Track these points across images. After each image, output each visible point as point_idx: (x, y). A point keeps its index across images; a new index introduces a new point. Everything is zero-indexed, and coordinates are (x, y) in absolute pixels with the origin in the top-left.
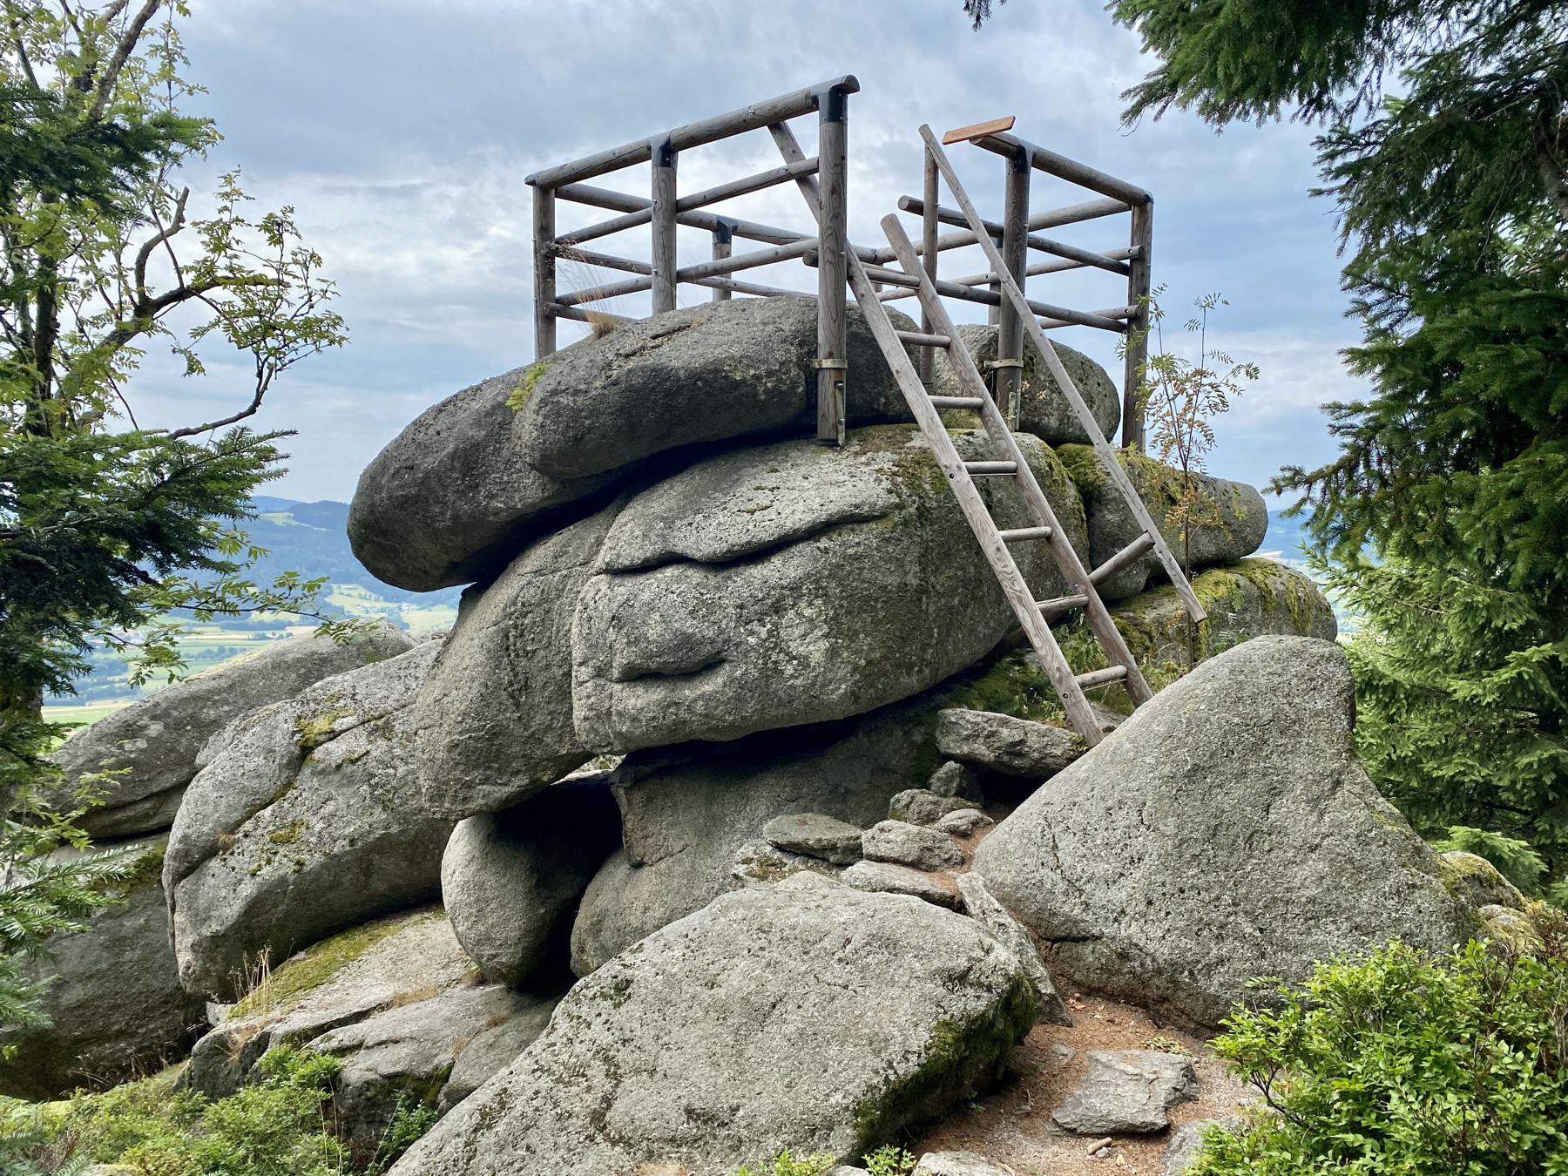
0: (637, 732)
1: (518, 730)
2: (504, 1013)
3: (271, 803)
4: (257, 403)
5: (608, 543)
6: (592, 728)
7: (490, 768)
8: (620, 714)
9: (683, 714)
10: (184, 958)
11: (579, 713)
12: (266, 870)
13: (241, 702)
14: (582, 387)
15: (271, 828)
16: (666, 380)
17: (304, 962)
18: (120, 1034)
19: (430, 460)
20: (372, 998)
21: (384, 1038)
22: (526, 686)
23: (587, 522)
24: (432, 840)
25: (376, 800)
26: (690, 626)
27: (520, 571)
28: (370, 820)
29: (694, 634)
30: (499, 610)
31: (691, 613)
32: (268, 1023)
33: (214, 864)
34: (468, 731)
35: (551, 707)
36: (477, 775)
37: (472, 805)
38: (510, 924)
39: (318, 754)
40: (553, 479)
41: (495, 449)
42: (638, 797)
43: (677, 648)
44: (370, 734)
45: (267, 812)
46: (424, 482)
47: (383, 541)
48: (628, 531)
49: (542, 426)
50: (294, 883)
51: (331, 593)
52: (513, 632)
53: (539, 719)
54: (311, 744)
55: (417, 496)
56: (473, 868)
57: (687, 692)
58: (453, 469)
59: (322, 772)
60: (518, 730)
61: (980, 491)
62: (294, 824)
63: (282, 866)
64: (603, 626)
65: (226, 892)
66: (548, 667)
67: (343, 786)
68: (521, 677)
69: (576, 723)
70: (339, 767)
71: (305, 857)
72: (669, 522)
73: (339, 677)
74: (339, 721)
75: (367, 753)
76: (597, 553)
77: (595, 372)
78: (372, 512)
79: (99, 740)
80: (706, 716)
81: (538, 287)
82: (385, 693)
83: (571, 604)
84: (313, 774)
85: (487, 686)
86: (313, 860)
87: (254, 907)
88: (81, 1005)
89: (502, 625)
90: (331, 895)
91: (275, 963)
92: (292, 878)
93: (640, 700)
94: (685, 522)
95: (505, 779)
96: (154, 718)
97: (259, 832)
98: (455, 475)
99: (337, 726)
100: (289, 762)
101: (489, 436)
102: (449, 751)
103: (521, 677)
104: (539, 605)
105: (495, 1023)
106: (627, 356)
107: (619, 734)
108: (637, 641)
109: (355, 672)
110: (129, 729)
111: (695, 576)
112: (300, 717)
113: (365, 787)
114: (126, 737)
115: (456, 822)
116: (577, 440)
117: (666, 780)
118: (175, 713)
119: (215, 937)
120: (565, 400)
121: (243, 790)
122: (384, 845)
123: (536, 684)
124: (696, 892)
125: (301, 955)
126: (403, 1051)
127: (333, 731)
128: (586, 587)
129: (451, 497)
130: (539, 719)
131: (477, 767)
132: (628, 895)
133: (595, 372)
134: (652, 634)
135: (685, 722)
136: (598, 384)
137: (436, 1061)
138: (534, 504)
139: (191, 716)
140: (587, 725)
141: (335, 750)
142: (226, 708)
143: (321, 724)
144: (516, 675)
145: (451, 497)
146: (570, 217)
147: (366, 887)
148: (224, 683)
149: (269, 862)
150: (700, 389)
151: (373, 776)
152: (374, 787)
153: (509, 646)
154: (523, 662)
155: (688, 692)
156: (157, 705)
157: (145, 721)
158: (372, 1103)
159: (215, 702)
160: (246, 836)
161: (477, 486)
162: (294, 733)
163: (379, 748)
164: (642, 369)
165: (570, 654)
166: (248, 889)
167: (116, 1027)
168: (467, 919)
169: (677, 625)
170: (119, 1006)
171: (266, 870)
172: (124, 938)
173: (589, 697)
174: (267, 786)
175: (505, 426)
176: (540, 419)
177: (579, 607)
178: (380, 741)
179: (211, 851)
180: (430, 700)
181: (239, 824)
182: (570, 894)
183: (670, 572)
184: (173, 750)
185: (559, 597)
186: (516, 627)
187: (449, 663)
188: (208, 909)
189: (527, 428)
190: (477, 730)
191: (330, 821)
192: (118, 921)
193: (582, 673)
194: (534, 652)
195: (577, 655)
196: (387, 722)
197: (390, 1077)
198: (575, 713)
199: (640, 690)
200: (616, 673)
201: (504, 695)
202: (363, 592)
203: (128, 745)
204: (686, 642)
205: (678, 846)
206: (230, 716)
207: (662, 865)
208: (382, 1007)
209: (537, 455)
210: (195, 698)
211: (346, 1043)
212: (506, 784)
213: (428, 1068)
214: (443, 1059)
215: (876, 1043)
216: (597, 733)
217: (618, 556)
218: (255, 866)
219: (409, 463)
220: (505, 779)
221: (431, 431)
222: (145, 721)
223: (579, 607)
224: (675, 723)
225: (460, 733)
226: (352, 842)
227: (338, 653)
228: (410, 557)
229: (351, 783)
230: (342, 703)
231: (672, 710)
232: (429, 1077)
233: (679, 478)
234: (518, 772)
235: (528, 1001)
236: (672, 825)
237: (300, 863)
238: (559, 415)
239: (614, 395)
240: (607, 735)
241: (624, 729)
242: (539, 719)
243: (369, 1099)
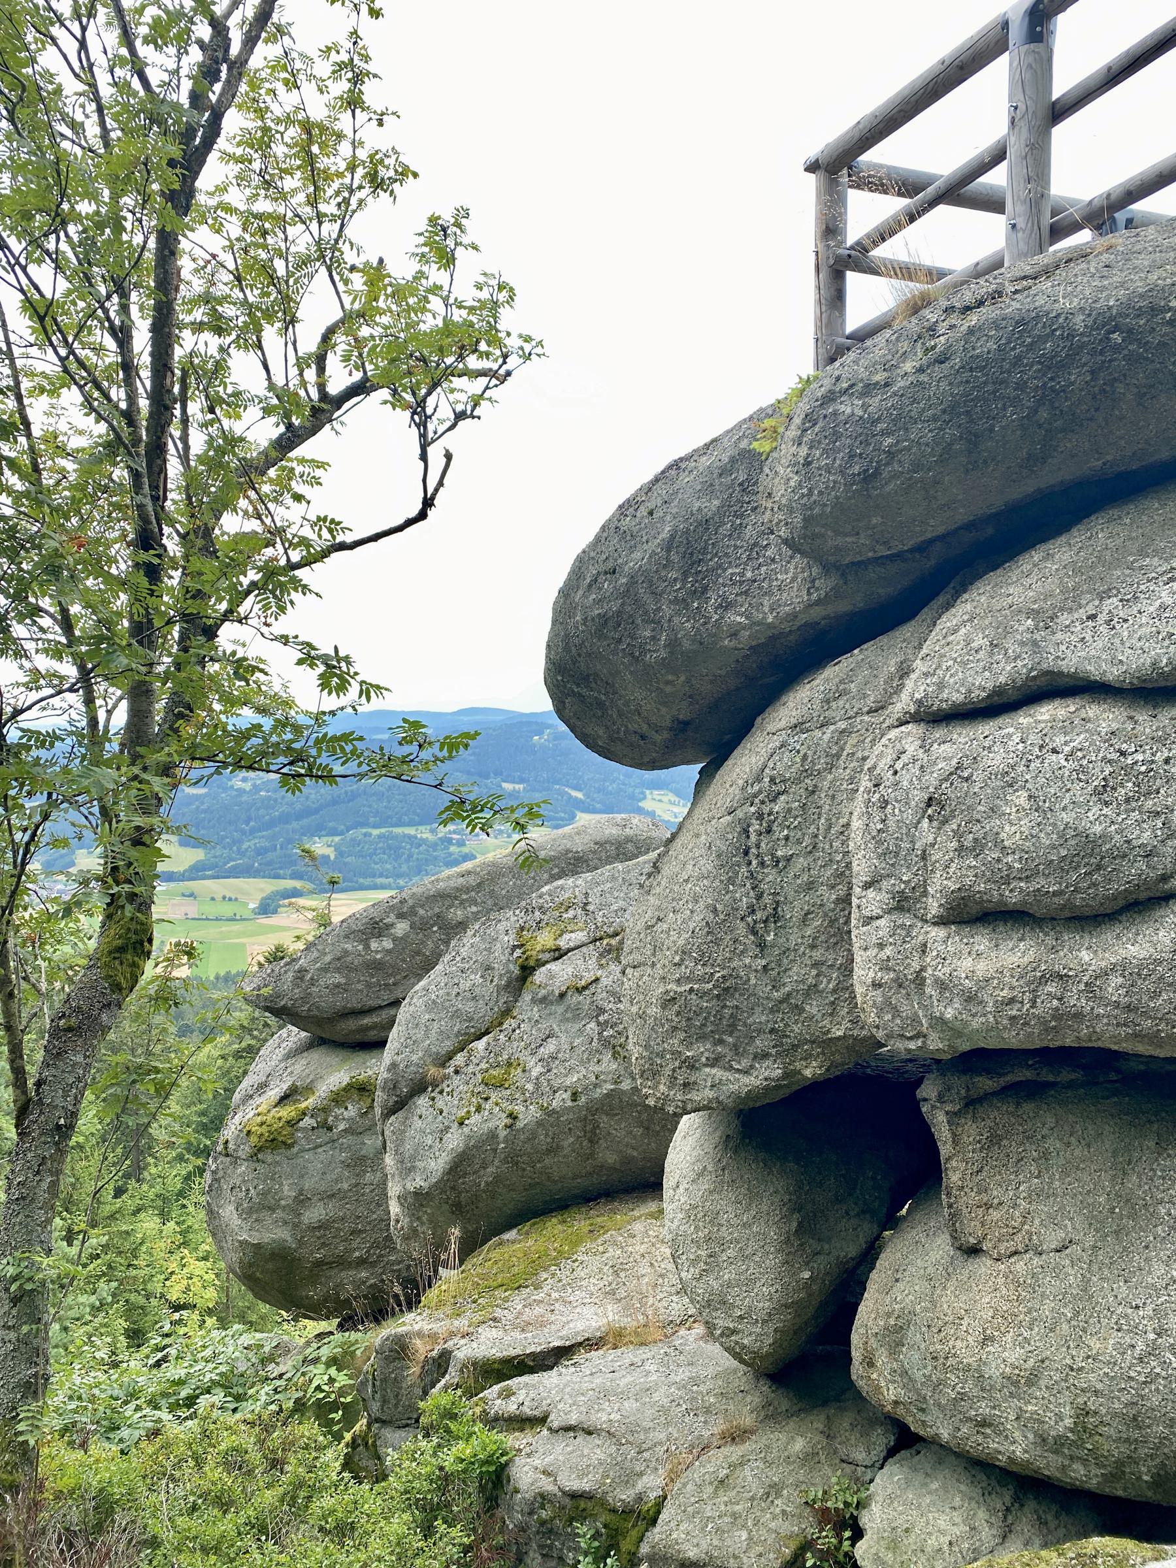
0: (976, 1023)
1: (763, 988)
2: (748, 1421)
3: (487, 1032)
4: (428, 503)
5: (919, 666)
6: (887, 1002)
7: (721, 1042)
8: (942, 986)
9: (1075, 999)
10: (394, 1208)
11: (863, 973)
12: (475, 1119)
13: (490, 902)
14: (879, 377)
15: (484, 1066)
16: (1043, 339)
17: (515, 1245)
18: (362, 1262)
19: (637, 555)
20: (580, 1326)
21: (573, 1420)
22: (776, 916)
23: (883, 640)
24: (662, 1125)
25: (606, 1043)
26: (1095, 820)
27: (771, 728)
28: (597, 1069)
29: (1105, 837)
30: (735, 791)
31: (1096, 792)
32: (452, 1334)
33: (422, 1101)
34: (688, 979)
35: (817, 954)
36: (702, 1050)
37: (695, 1096)
38: (762, 1284)
39: (539, 976)
40: (827, 568)
41: (734, 528)
42: (971, 1131)
43: (1068, 864)
44: (601, 955)
45: (481, 1045)
46: (627, 592)
47: (584, 691)
48: (961, 645)
49: (807, 463)
50: (506, 1140)
51: (645, 798)
52: (755, 826)
53: (797, 974)
54: (532, 963)
55: (619, 613)
56: (705, 1185)
57: (1085, 956)
58: (668, 564)
59: (544, 1000)
60: (763, 988)
61: (290, 1088)
62: (509, 1064)
63: (491, 1119)
64: (909, 816)
65: (427, 1145)
66: (810, 886)
67: (568, 1020)
68: (767, 899)
69: (859, 990)
70: (562, 995)
71: (519, 1108)
72: (1045, 619)
73: (570, 881)
74: (566, 936)
75: (597, 980)
76: (898, 690)
77: (905, 346)
78: (567, 649)
79: (347, 937)
80: (1129, 1008)
81: (819, 319)
82: (621, 903)
83: (851, 780)
84: (534, 1001)
85: (715, 911)
86: (529, 1115)
87: (460, 1165)
88: (323, 1226)
89: (740, 814)
90: (547, 1161)
91: (469, 1247)
92: (503, 1134)
93: (990, 964)
94: (1082, 614)
95: (745, 1063)
96: (401, 916)
97: (471, 1069)
98: (673, 575)
99: (563, 943)
100: (508, 985)
101: (726, 505)
102: (664, 1007)
103: (767, 899)
104: (797, 781)
105: (734, 1436)
106: (967, 309)
107: (939, 1022)
108: (978, 848)
109: (588, 876)
110: (374, 927)
111: (1106, 717)
112: (522, 929)
113: (593, 1025)
114: (373, 935)
115: (677, 1117)
116: (868, 478)
117: (1028, 1107)
118: (421, 912)
119: (417, 1194)
120: (847, 407)
121: (457, 1014)
122: (614, 1104)
123: (792, 912)
124: (1095, 1345)
125: (511, 1235)
126: (595, 1451)
127: (558, 949)
128: (878, 749)
129: (667, 610)
130: (797, 974)
131: (702, 1038)
132: (950, 1301)
133: (905, 346)
134: (1010, 834)
135: (1078, 1016)
136: (908, 366)
137: (640, 1486)
138: (794, 616)
140: (878, 996)
141: (557, 974)
142: (474, 909)
143: (545, 939)
144: (759, 897)
145: (667, 610)
146: (865, 212)
147: (591, 1155)
148: (472, 881)
149: (479, 1109)
150: (1117, 348)
151: (602, 1011)
152: (603, 1026)
153: (745, 852)
154: (771, 875)
155: (1087, 954)
156: (403, 901)
157: (391, 919)
158: (547, 1529)
160: (457, 1072)
161: (705, 589)
162: (515, 947)
163: (610, 975)
164: (996, 324)
165: (849, 865)
166: (455, 1140)
167: (357, 1254)
168: (694, 1262)
169: (1067, 817)
170: (360, 1231)
171: (475, 1119)
172: (364, 1158)
173: (881, 946)
174: (483, 1012)
175: (748, 487)
176: (804, 451)
177: (865, 783)
178: (612, 967)
179: (420, 1087)
180: (640, 926)
181: (450, 1056)
182: (852, 1250)
183: (1046, 712)
184: (418, 953)
185: (830, 767)
186: (760, 816)
187: (667, 870)
188: (413, 1158)
189: (781, 482)
190: (701, 980)
191: (551, 1068)
192: (359, 1139)
193: (870, 901)
194: (789, 859)
195: (861, 869)
197: (574, 1496)
198: (858, 972)
199: (982, 941)
200: (933, 907)
201: (741, 929)
202: (673, 798)
203: (374, 945)
204: (1088, 850)
205: (1053, 1238)
206: (476, 917)
207: (1020, 1266)
208: (592, 1344)
209: (798, 520)
210: (441, 896)
211: (527, 1411)
212: (746, 1072)
213: (625, 1495)
214: (651, 1484)
216: (896, 1012)
217: (941, 686)
218: (462, 1113)
219: (610, 564)
220: (745, 1063)
221: (643, 511)
222: (391, 919)
223: (865, 783)
224: (1057, 1015)
225: (678, 982)
226: (575, 1096)
227: (595, 852)
228: (620, 714)
229: (577, 1018)
230: (571, 913)
231: (1051, 988)
232: (627, 1512)
233: (1063, 539)
234: (765, 1056)
235: (785, 1405)
236: (1035, 1195)
237: (513, 1116)
238: (837, 436)
239: (940, 384)
240: (915, 1019)
241: (949, 1014)
242: (796, 972)
243: (543, 1523)
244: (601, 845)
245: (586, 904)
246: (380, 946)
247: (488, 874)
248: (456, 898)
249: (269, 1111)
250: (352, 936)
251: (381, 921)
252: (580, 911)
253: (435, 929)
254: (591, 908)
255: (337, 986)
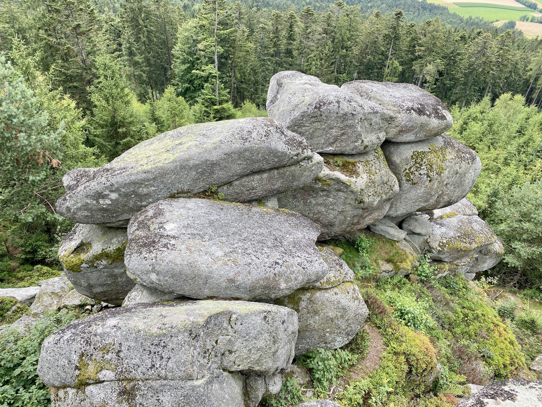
79: (87, 197)
96: (112, 191)
99: (101, 376)
118: (123, 190)
139: (133, 191)
142: (153, 188)
148: (150, 176)
159: (146, 185)
196: (133, 388)
203: (101, 202)
210: (134, 183)
215: (348, 88)
244: (229, 155)
245: (119, 351)
246: (105, 203)
247: (159, 173)
248: (142, 184)
249: (69, 256)
250: (89, 197)
251: (102, 192)
252: (114, 355)
253: (133, 196)
254: (121, 354)
255: (87, 216)
